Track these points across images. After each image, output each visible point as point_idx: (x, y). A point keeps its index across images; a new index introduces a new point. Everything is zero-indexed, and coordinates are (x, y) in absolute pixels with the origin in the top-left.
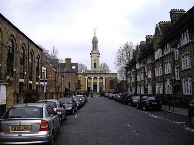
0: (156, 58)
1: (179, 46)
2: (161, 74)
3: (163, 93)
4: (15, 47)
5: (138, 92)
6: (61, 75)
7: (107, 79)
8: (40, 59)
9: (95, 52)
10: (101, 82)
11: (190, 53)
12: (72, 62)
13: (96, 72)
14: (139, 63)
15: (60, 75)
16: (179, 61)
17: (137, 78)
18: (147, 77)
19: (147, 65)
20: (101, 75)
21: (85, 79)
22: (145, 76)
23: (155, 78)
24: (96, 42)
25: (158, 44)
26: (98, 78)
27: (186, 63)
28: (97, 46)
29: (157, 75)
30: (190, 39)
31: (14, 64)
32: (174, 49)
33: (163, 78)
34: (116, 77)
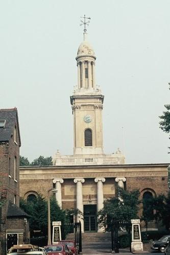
17: (96, 100)
20: (110, 170)
21: (54, 185)
24: (90, 60)
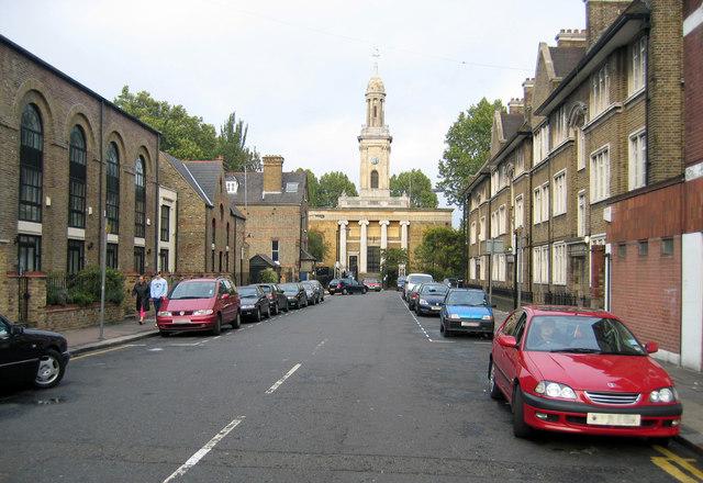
0: (537, 160)
4: (47, 129)
5: (540, 276)
6: (232, 214)
7: (414, 228)
9: (374, 131)
10: (393, 238)
12: (287, 168)
13: (374, 202)
14: (496, 175)
15: (227, 214)
19: (515, 183)
22: (510, 219)
23: (533, 228)
26: (384, 222)
28: (382, 113)
29: (536, 220)
30: (611, 100)
31: (46, 183)
32: (576, 133)
34: (447, 220)
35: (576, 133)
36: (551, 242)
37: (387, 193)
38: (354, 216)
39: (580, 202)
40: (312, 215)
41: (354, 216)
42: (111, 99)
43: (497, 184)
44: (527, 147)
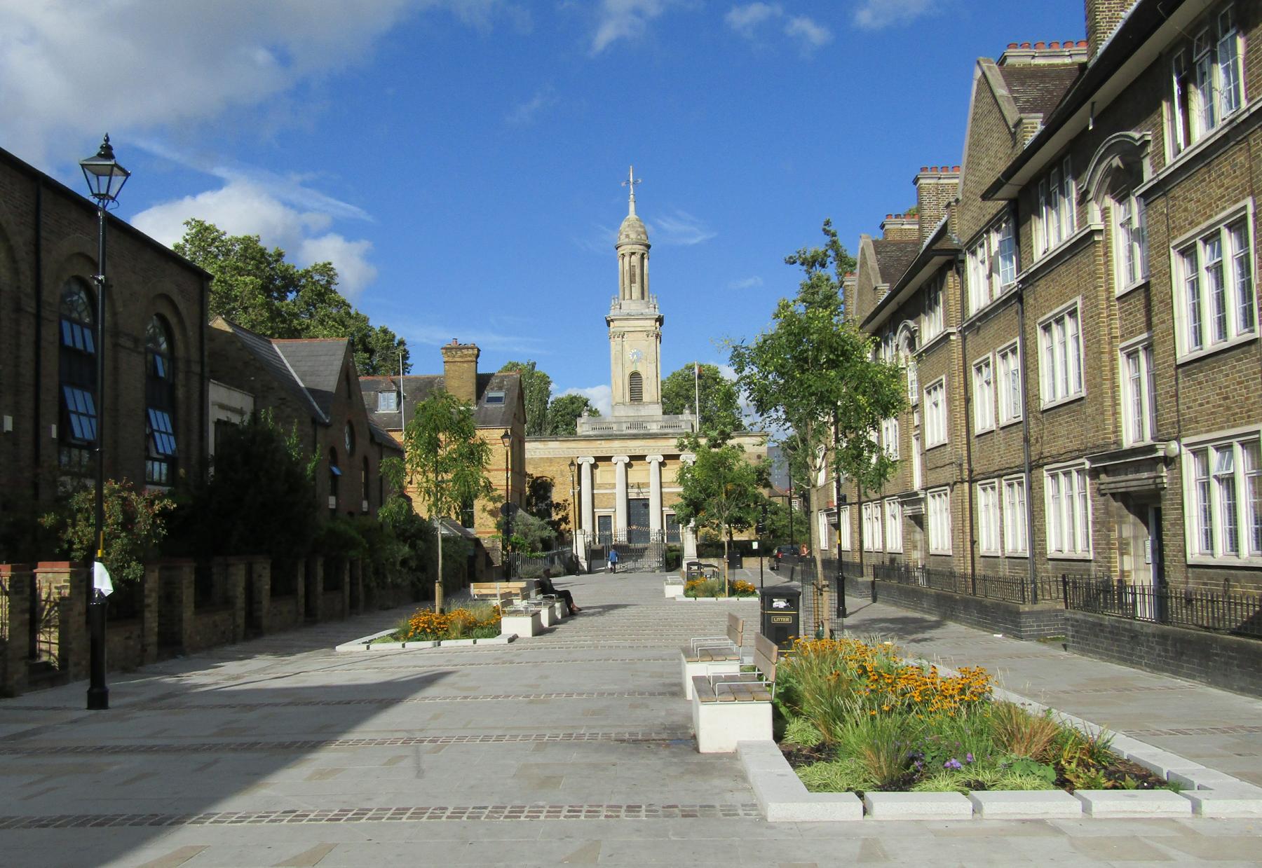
1: (1148, 173)
2: (1010, 411)
3: (1033, 548)
6: (372, 439)
8: (184, 329)
11: (1250, 210)
16: (1149, 299)
18: (921, 437)
21: (580, 466)
25: (986, 196)
27: (1201, 314)
29: (983, 421)
32: (1105, 213)
33: (1026, 440)
35: (1105, 213)
36: (1033, 466)
37: (657, 410)
38: (603, 448)
39: (915, 445)
40: (534, 450)
41: (603, 448)
42: (170, 246)
43: (984, 283)
44: (951, 279)
